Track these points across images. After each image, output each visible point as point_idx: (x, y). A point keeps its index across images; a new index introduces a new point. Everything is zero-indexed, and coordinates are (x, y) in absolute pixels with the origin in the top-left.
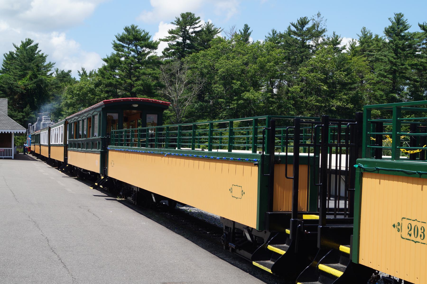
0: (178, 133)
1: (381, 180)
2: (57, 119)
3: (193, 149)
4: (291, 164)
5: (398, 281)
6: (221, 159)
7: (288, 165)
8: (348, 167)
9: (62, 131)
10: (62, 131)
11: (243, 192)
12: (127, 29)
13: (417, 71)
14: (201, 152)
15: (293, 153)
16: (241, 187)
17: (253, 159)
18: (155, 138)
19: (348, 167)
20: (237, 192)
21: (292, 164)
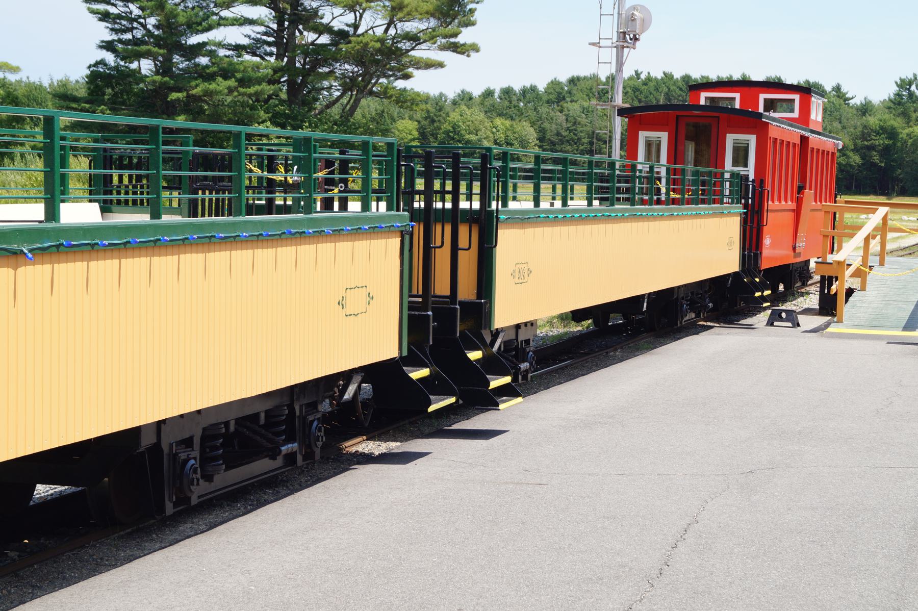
0: (569, 166)
1: (181, 255)
2: (131, 82)
3: (156, 215)
4: (448, 222)
5: (32, 503)
6: (320, 234)
7: (445, 224)
8: (750, 196)
9: (328, 153)
10: (328, 153)
11: (371, 296)
12: (837, 89)
13: (184, 42)
14: (150, 226)
15: (451, 204)
16: (366, 286)
17: (10, 244)
18: (542, 175)
19: (750, 196)
20: (356, 301)
21: (450, 222)
